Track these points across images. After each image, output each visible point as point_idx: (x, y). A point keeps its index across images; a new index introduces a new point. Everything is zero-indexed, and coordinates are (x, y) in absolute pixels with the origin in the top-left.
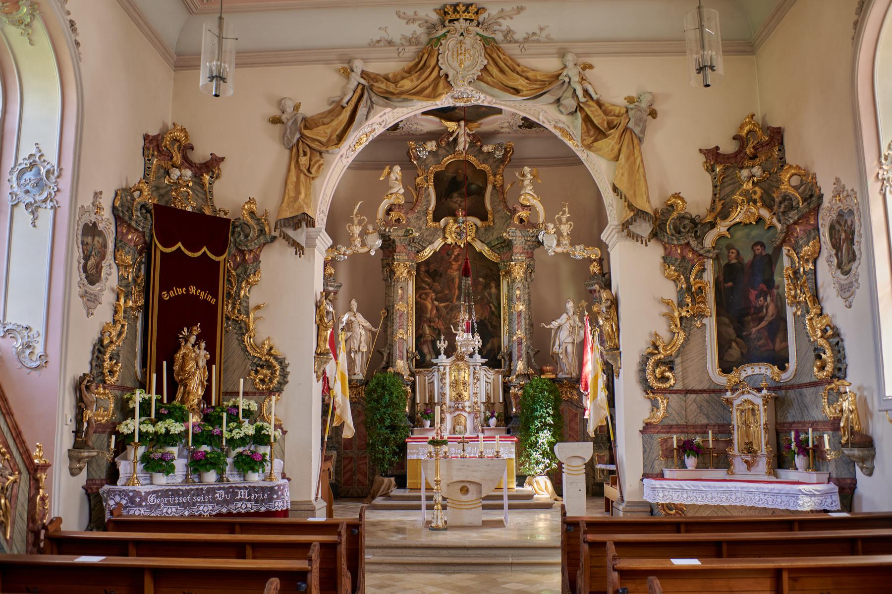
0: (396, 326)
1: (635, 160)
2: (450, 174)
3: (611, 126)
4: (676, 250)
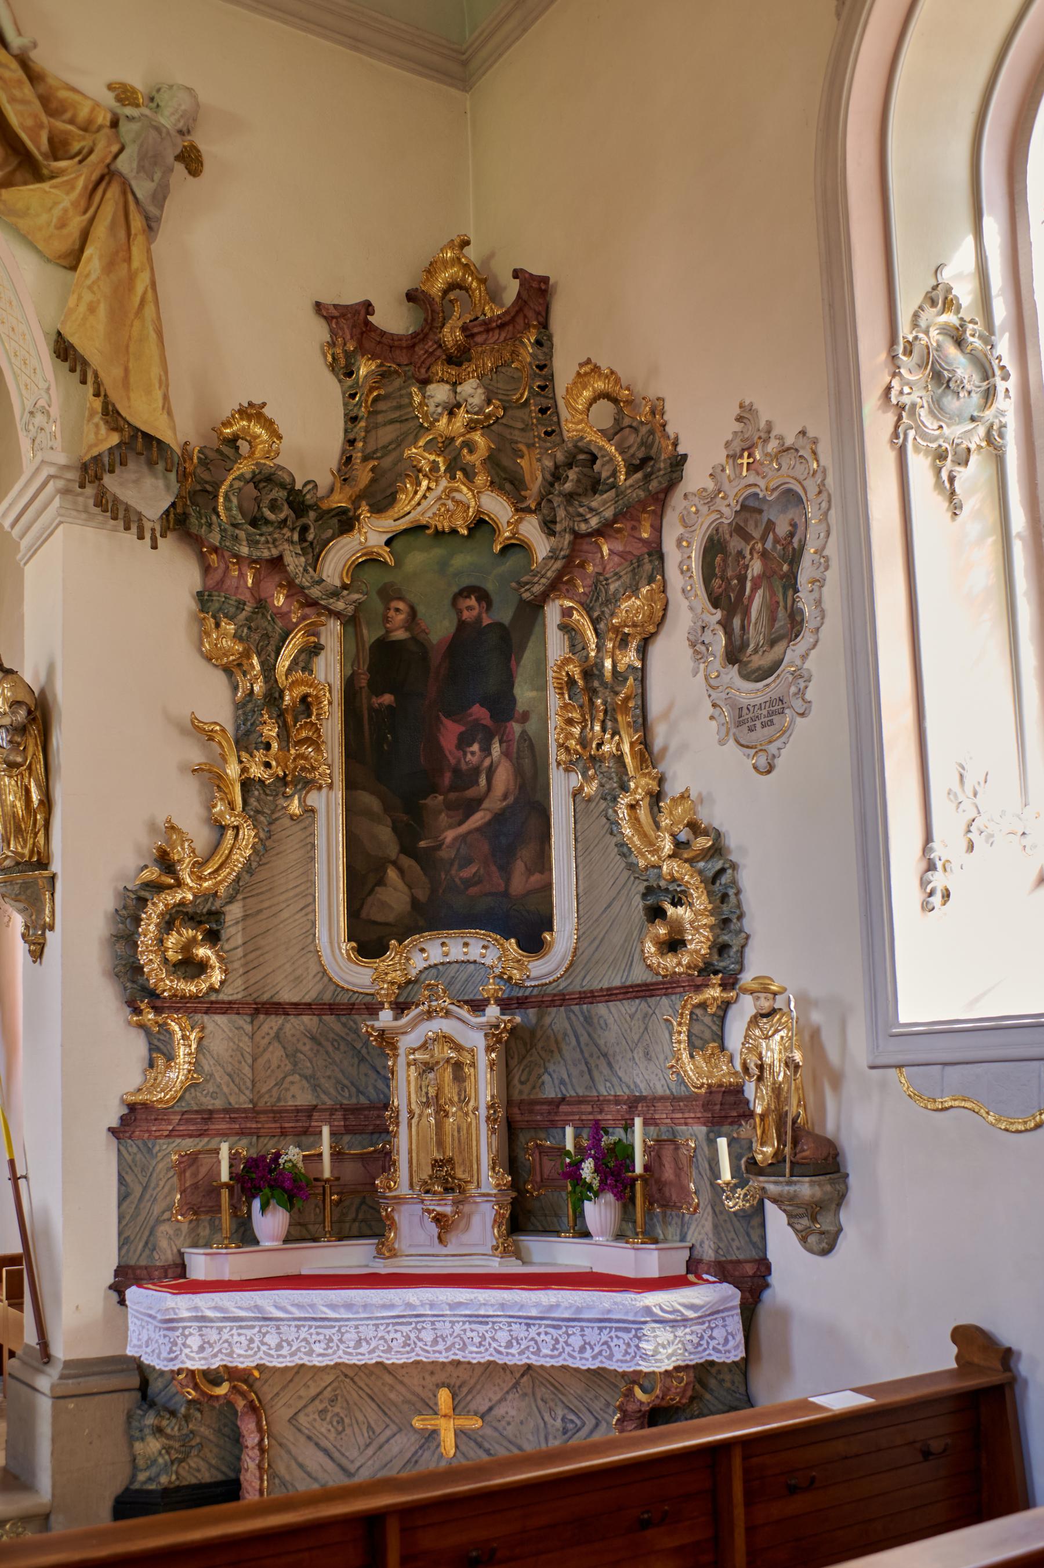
1: (132, 277)
3: (58, 148)
4: (242, 576)
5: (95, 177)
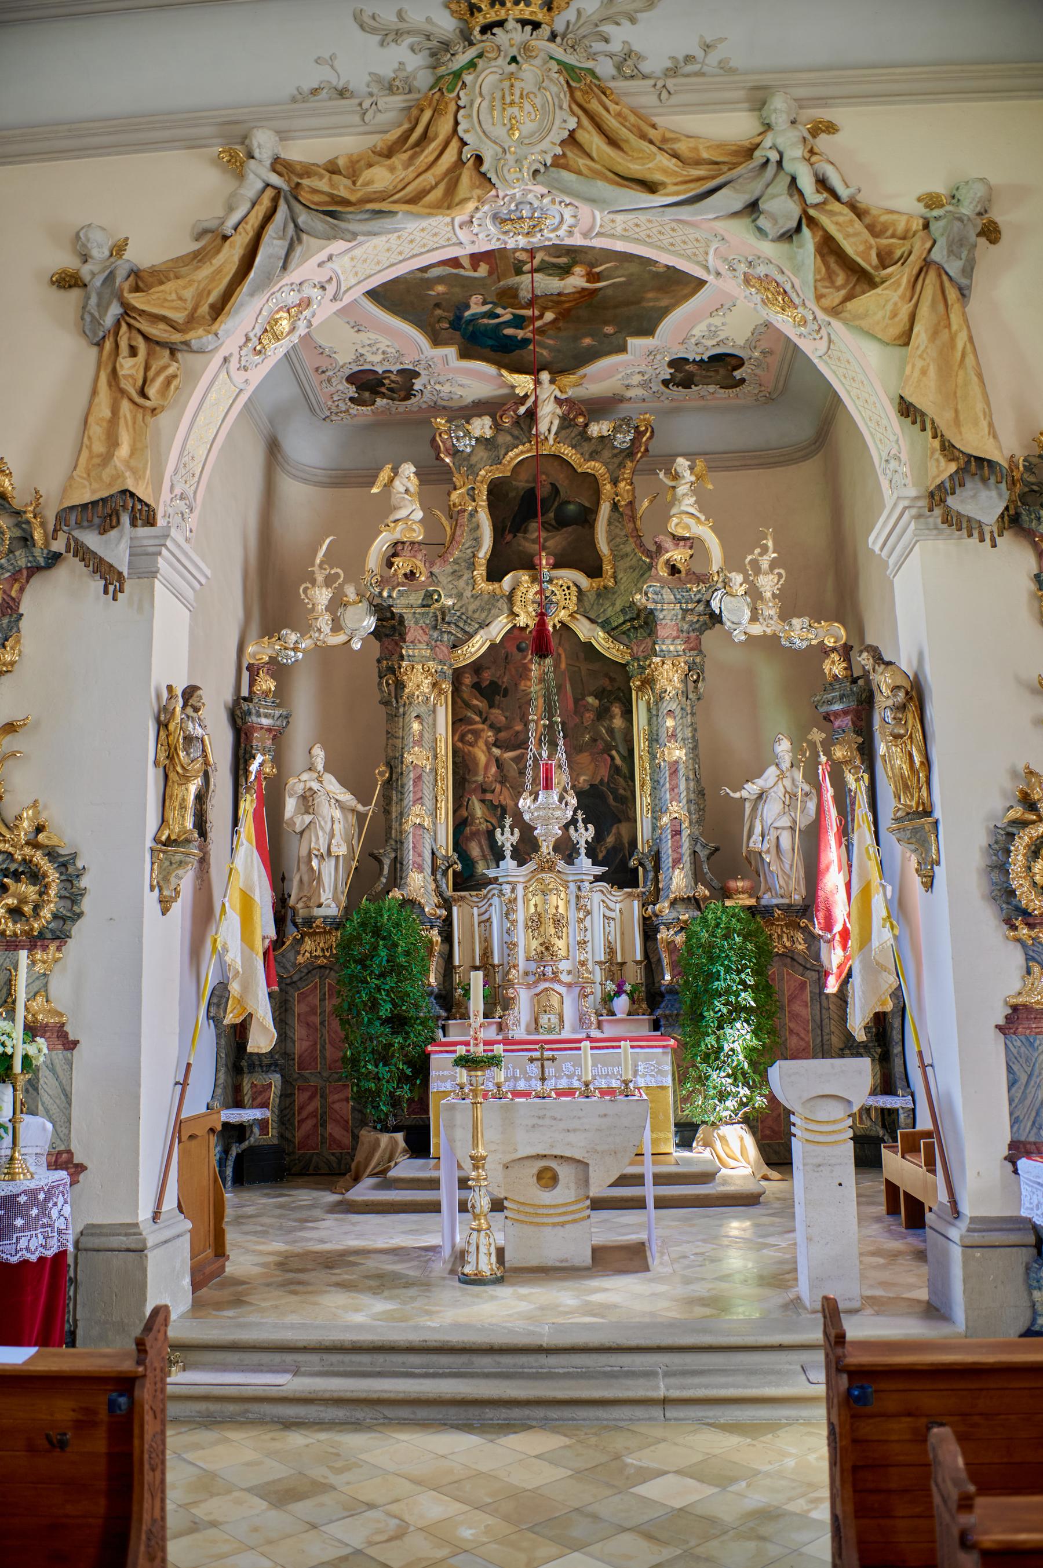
0: (410, 797)
1: (953, 339)
2: (522, 483)
3: (885, 259)
5: (915, 272)
